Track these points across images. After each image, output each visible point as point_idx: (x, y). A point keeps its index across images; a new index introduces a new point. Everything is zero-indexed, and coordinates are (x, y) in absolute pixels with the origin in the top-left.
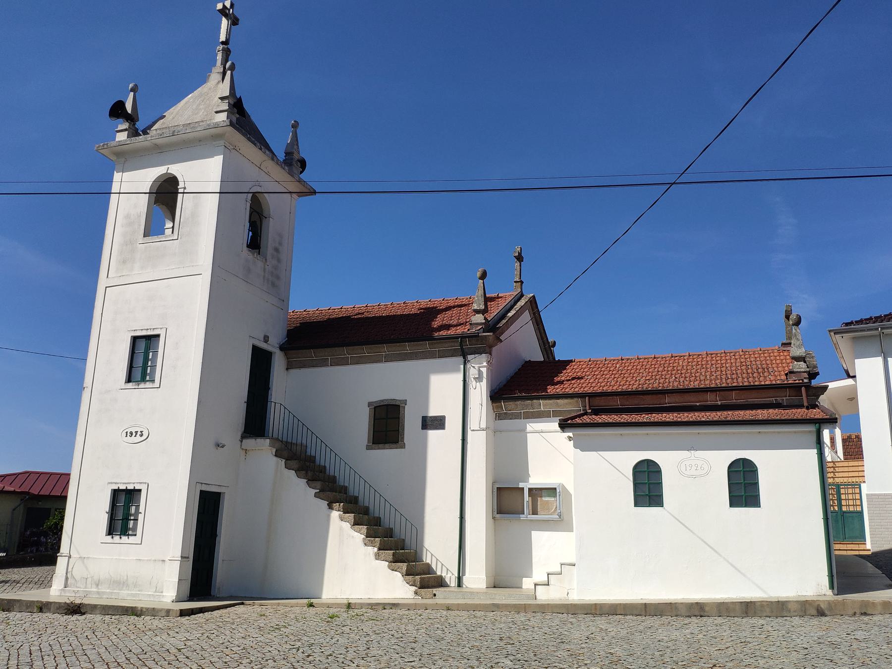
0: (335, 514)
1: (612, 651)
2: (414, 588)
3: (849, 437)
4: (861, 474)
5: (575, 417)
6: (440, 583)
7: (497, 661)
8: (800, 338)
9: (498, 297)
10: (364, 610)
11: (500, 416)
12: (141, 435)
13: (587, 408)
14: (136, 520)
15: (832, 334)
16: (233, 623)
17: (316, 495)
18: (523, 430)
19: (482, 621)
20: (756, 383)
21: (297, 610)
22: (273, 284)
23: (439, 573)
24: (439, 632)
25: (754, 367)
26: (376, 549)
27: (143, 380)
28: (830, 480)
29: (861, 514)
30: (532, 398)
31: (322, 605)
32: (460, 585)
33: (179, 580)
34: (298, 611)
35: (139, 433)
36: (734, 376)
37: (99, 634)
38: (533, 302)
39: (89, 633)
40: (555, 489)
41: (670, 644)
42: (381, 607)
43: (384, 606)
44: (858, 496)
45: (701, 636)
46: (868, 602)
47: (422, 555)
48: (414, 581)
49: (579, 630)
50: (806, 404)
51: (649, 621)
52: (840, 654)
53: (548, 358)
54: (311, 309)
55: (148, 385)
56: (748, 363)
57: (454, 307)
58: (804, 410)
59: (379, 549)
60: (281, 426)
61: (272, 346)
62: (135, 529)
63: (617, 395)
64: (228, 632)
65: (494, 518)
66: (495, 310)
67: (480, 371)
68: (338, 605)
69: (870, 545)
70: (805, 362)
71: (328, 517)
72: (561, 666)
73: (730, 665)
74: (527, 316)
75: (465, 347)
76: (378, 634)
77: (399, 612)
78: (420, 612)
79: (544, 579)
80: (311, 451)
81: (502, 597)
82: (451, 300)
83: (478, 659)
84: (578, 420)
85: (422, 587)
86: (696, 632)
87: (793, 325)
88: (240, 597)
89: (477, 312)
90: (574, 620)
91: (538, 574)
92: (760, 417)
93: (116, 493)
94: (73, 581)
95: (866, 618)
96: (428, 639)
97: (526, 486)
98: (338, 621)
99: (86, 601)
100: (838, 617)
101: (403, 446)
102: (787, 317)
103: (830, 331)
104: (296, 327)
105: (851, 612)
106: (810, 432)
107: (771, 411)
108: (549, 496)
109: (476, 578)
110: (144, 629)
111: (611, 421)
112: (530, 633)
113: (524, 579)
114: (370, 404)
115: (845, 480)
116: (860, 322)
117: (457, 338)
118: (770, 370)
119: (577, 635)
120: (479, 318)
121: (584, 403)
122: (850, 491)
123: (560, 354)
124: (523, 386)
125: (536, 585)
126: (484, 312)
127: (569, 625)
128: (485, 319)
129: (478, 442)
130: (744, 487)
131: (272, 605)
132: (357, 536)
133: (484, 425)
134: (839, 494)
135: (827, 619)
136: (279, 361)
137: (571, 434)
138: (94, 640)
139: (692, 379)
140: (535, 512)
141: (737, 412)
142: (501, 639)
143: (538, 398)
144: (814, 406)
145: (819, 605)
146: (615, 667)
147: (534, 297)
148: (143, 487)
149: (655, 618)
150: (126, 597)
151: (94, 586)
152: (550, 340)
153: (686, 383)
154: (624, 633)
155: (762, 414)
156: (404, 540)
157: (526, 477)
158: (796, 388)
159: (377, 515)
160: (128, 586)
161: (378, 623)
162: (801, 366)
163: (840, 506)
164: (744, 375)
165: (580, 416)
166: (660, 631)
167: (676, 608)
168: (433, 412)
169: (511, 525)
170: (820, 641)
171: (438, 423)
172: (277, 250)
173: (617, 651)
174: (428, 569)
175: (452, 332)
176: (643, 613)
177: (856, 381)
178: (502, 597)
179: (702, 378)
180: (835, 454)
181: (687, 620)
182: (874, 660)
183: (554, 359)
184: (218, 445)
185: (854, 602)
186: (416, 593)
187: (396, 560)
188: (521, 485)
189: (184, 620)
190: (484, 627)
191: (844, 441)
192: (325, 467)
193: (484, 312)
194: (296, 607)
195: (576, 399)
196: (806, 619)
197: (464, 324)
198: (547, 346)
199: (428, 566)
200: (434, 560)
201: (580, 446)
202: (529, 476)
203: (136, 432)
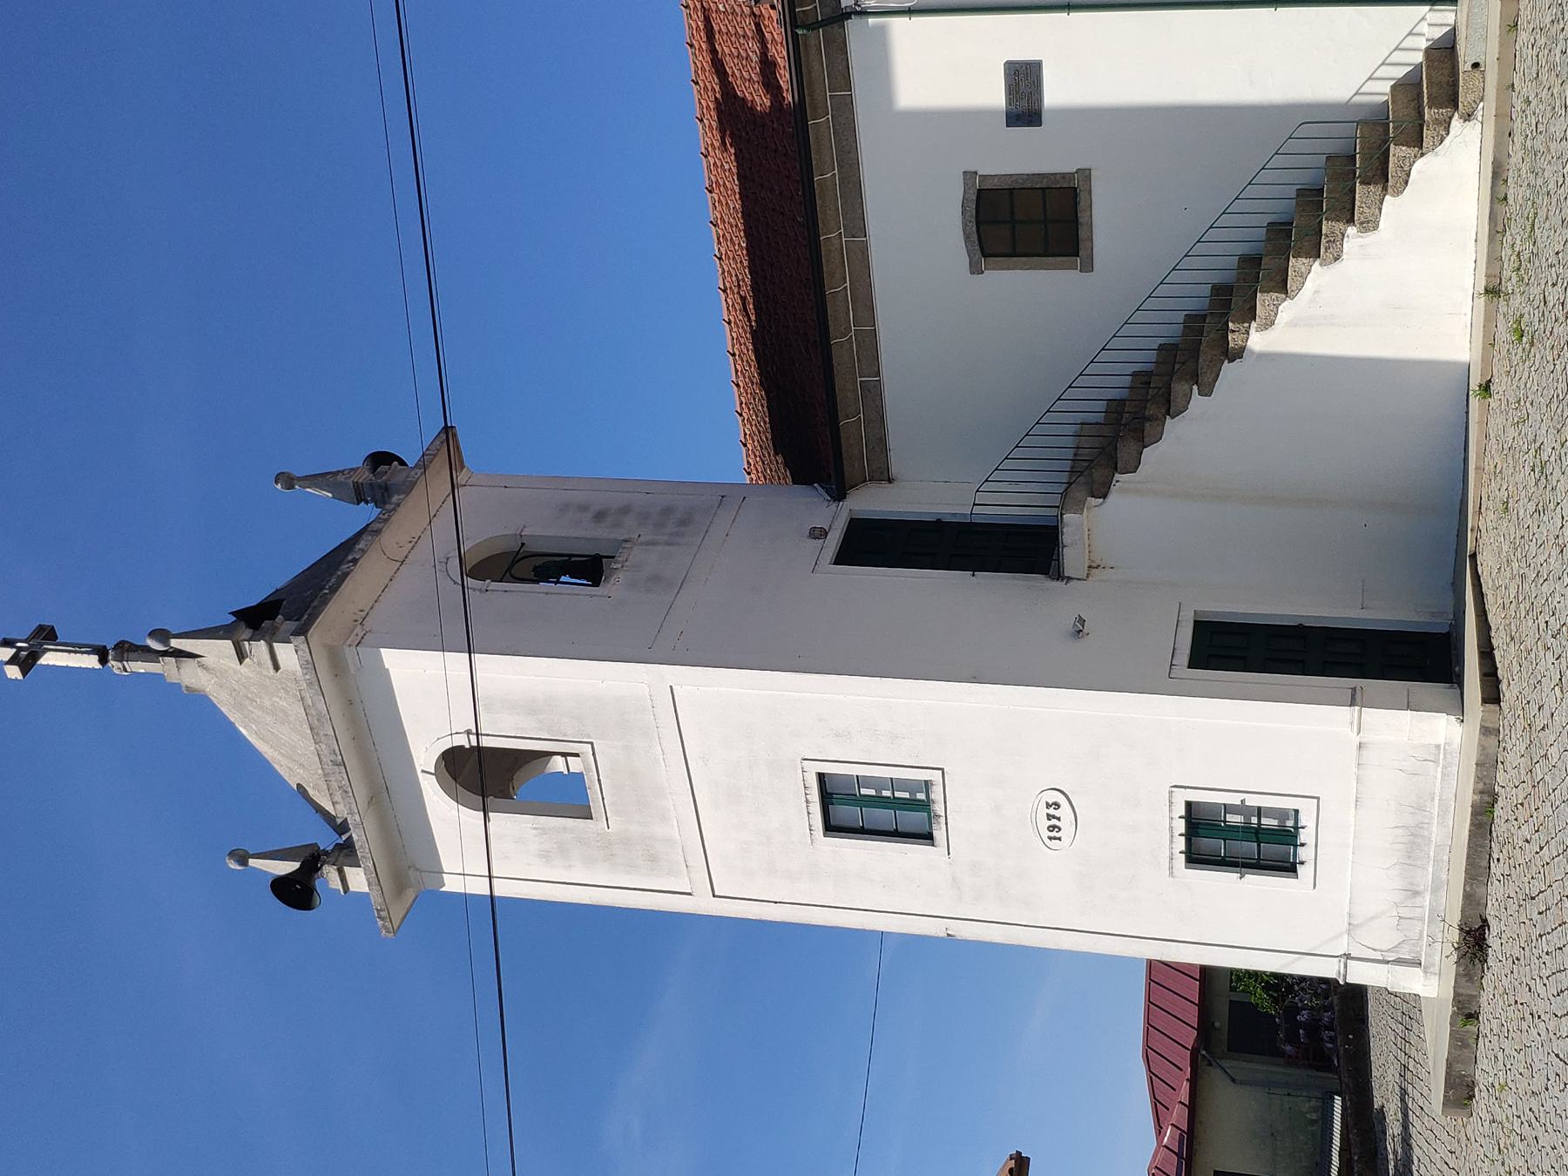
0: (1257, 340)
2: (1456, 123)
6: (1444, 52)
10: (1506, 253)
12: (1057, 805)
14: (1259, 811)
17: (1207, 391)
21: (1496, 421)
22: (684, 522)
23: (1419, 58)
26: (1351, 230)
27: (925, 806)
31: (1487, 360)
34: (1500, 420)
35: (1052, 811)
37: (1538, 885)
39: (1532, 910)
42: (1501, 208)
43: (1498, 199)
48: (1437, 122)
54: (739, 429)
55: (937, 794)
57: (713, 51)
61: (835, 518)
62: (1281, 814)
68: (1490, 320)
80: (1095, 411)
82: (691, 62)
85: (1453, 102)
88: (1456, 561)
93: (1195, 858)
94: (1406, 948)
98: (1531, 318)
99: (1455, 917)
101: (1085, 174)
104: (786, 465)
114: (975, 269)
117: (795, 37)
131: (1479, 484)
136: (870, 502)
148: (1182, 797)
150: (1449, 831)
151: (1418, 900)
160: (1419, 826)
161: (1542, 214)
168: (994, 95)
171: (1024, 79)
172: (600, 516)
174: (1408, 88)
186: (1468, 117)
189: (1508, 693)
192: (1134, 374)
199: (1399, 87)
203: (1049, 817)
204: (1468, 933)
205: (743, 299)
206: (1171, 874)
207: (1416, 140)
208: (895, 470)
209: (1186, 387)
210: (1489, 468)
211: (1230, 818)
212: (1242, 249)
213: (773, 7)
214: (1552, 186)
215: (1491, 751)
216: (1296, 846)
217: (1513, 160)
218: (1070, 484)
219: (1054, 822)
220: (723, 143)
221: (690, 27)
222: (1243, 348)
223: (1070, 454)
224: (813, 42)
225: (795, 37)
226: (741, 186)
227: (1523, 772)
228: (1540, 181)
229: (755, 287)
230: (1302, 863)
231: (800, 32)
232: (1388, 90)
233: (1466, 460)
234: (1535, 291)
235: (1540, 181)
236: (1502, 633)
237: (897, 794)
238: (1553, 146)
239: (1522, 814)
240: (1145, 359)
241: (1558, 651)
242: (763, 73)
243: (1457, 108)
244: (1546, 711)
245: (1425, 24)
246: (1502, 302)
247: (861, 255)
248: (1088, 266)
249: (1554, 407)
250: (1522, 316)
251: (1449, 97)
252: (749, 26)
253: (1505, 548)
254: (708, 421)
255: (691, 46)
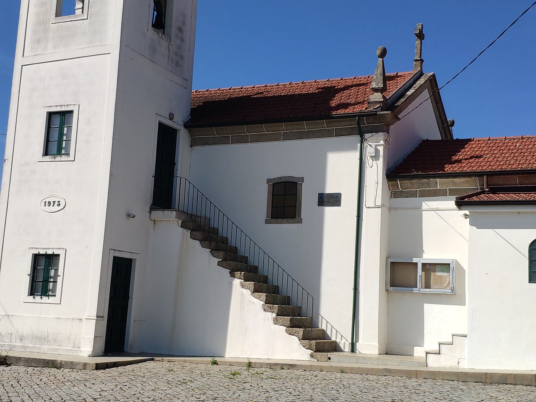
0: (237, 282)
2: (310, 352)
5: (472, 195)
6: (335, 348)
10: (264, 369)
11: (395, 194)
13: (485, 186)
14: (55, 282)
16: (144, 377)
17: (219, 264)
18: (419, 208)
21: (202, 367)
22: (177, 64)
23: (333, 339)
26: (274, 315)
27: (59, 153)
30: (428, 177)
31: (225, 363)
32: (353, 350)
33: (95, 337)
34: (203, 368)
35: (56, 203)
37: (23, 384)
38: (433, 80)
39: (14, 383)
40: (449, 264)
42: (279, 367)
43: (282, 366)
47: (318, 322)
48: (310, 345)
53: (446, 136)
54: (213, 89)
55: (64, 158)
57: (352, 86)
59: (278, 315)
60: (186, 200)
61: (177, 123)
62: (54, 290)
63: (515, 174)
64: (139, 385)
66: (393, 89)
67: (376, 149)
68: (240, 364)
71: (231, 284)
74: (426, 94)
75: (362, 125)
76: (276, 391)
77: (296, 372)
79: (436, 348)
80: (214, 224)
81: (393, 363)
82: (349, 78)
84: (475, 199)
85: (317, 351)
88: (151, 354)
89: (376, 90)
91: (430, 343)
93: (36, 258)
97: (419, 261)
98: (239, 378)
99: (11, 354)
101: (300, 221)
104: (198, 106)
108: (442, 271)
109: (369, 345)
110: (63, 380)
111: (509, 199)
113: (415, 347)
114: (269, 181)
117: (355, 116)
120: (377, 97)
121: (481, 182)
123: (458, 133)
124: (419, 165)
125: (427, 353)
126: (382, 90)
127: (460, 392)
128: (384, 97)
129: (373, 219)
131: (179, 361)
132: (257, 303)
133: (379, 203)
136: (183, 138)
137: (467, 212)
138: (19, 388)
140: (428, 286)
147: (434, 75)
148: (61, 253)
150: (46, 352)
151: (18, 341)
152: (449, 119)
157: (420, 252)
159: (275, 283)
160: (48, 341)
161: (277, 381)
165: (477, 194)
168: (330, 189)
169: (404, 298)
171: (334, 200)
172: (180, 30)
174: (323, 335)
175: (349, 111)
178: (393, 363)
184: (129, 215)
186: (312, 356)
187: (293, 325)
188: (415, 260)
189: (100, 373)
190: (377, 390)
192: (227, 238)
193: (382, 90)
194: (200, 364)
195: (473, 178)
198: (445, 125)
199: (324, 332)
200: (329, 327)
203: (54, 202)
204: (5, 359)
205: (262, 93)
206: (30, 248)
207: (305, 338)
208: (197, 148)
209: (221, 257)
210: (186, 365)
211: (53, 271)
212: (270, 277)
213: (366, 108)
214: (286, 384)
215: (78, 367)
216: (41, 295)
217: (296, 371)
218: (187, 214)
219: (52, 204)
220: (319, 88)
221: (361, 78)
222: (234, 277)
223: (199, 214)
224: (353, 123)
225: (355, 116)
226: (310, 94)
227: (68, 378)
228: (288, 380)
229: (266, 98)
230: (34, 298)
231: (357, 118)
232: (323, 328)
233: (189, 356)
234: (249, 379)
235: (288, 380)
236: (123, 370)
237: (64, 142)
238: (300, 385)
239: (52, 378)
240: (233, 242)
241: (115, 390)
242: (343, 104)
243: (315, 352)
244: (92, 386)
245: (345, 341)
246: (245, 368)
247: (277, 139)
248: (267, 222)
249: (207, 386)
250: (240, 375)
251: (319, 349)
252: (360, 99)
253: (155, 371)
254: (218, 76)
255: (355, 78)
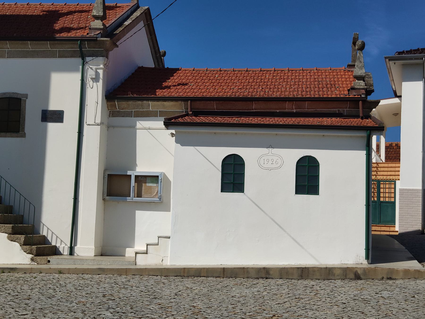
1: (195, 305)
2: (31, 256)
3: (391, 145)
4: (397, 173)
7: (99, 313)
8: (362, 61)
9: (116, 7)
13: (189, 110)
15: (387, 60)
18: (133, 127)
19: (89, 282)
20: (325, 96)
23: (53, 244)
24: (51, 291)
25: (324, 83)
28: (373, 177)
29: (394, 203)
32: (71, 252)
36: (308, 90)
38: (147, 14)
40: (158, 176)
41: (241, 299)
44: (393, 191)
45: (265, 293)
46: (393, 269)
49: (168, 289)
50: (361, 115)
51: (230, 282)
52: (370, 308)
53: (158, 64)
56: (320, 80)
57: (75, 12)
58: (360, 119)
65: (104, 199)
66: (113, 18)
69: (398, 228)
70: (364, 81)
72: (153, 316)
73: (286, 315)
75: (84, 49)
77: (16, 275)
78: (35, 275)
81: (107, 263)
82: (72, 5)
83: (83, 312)
84: (180, 120)
85: (37, 255)
86: (262, 290)
87: (358, 49)
89: (96, 18)
90: (166, 281)
91: (140, 246)
92: (325, 123)
95: (391, 282)
96: (41, 296)
100: (371, 280)
102: (354, 43)
103: (386, 58)
105: (380, 277)
106: (362, 137)
107: (334, 119)
108: (152, 182)
111: (207, 121)
112: (129, 291)
113: (127, 249)
115: (385, 177)
116: (410, 52)
117: (77, 40)
118: (337, 86)
119: (168, 292)
121: (186, 105)
122: (387, 186)
123: (169, 63)
125: (136, 253)
127: (162, 285)
128: (104, 25)
129: (93, 136)
130: (307, 179)
133: (98, 121)
134: (379, 188)
135: (362, 281)
137: (173, 131)
139: (275, 90)
140: (139, 195)
141: (307, 119)
142: (104, 296)
143: (148, 99)
144: (368, 116)
145: (356, 271)
146: (196, 317)
147: (148, 9)
149: (231, 279)
152: (161, 50)
153: (270, 93)
154: (205, 290)
155: (326, 121)
156: (23, 216)
157: (133, 166)
158: (355, 102)
162: (361, 84)
163: (379, 197)
164: (316, 89)
165: (182, 116)
166: (234, 289)
167: (248, 272)
168: (53, 107)
169: (119, 206)
170: (355, 298)
171: (58, 117)
173: (199, 304)
175: (72, 34)
176: (222, 275)
177: (401, 100)
178: (107, 263)
179: (283, 89)
180: (379, 157)
181: (255, 281)
182: (394, 313)
183: (164, 66)
185: (383, 269)
186: (32, 260)
188: (129, 173)
190: (90, 287)
191: (387, 148)
193: (103, 18)
195: (180, 102)
196: (346, 281)
197: (84, 28)
199: (45, 238)
201: (181, 141)
202: (136, 165)
